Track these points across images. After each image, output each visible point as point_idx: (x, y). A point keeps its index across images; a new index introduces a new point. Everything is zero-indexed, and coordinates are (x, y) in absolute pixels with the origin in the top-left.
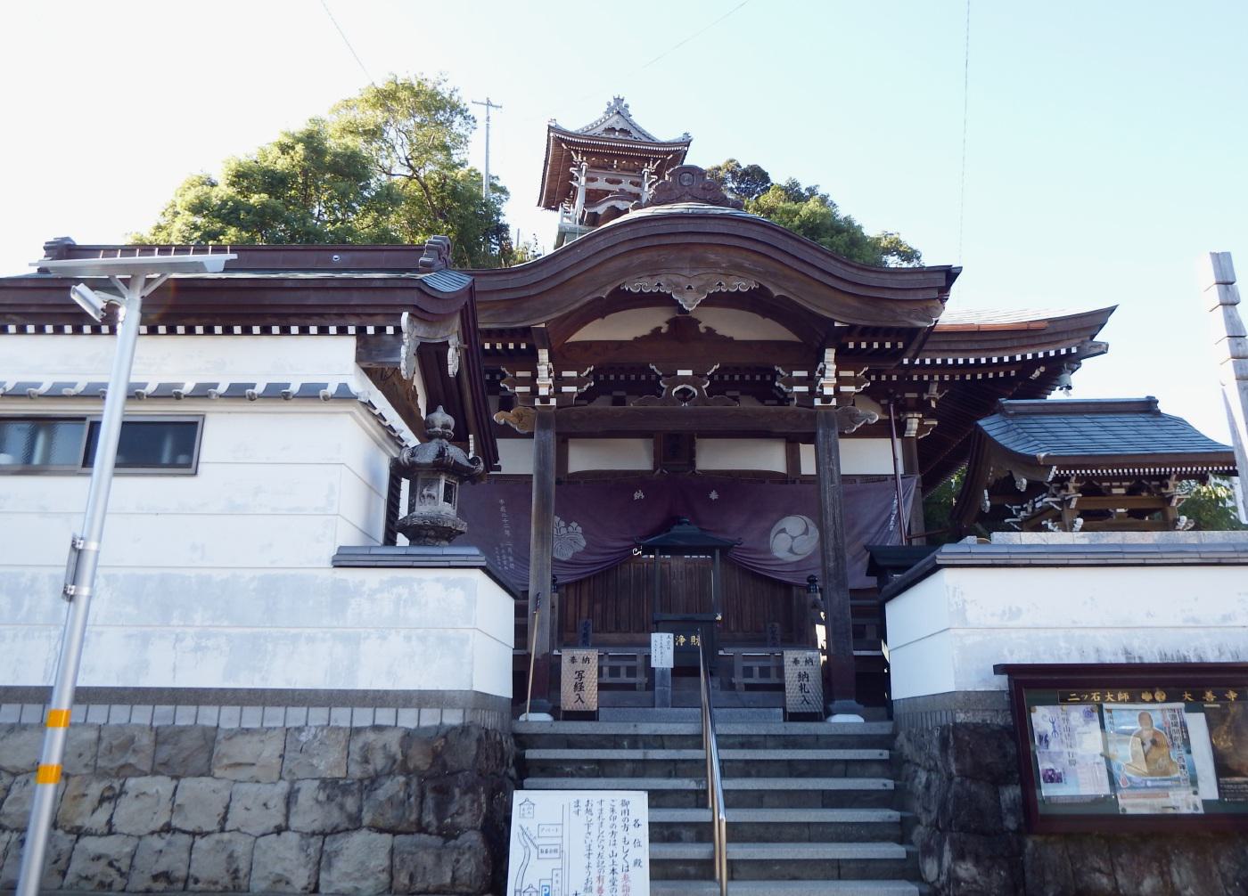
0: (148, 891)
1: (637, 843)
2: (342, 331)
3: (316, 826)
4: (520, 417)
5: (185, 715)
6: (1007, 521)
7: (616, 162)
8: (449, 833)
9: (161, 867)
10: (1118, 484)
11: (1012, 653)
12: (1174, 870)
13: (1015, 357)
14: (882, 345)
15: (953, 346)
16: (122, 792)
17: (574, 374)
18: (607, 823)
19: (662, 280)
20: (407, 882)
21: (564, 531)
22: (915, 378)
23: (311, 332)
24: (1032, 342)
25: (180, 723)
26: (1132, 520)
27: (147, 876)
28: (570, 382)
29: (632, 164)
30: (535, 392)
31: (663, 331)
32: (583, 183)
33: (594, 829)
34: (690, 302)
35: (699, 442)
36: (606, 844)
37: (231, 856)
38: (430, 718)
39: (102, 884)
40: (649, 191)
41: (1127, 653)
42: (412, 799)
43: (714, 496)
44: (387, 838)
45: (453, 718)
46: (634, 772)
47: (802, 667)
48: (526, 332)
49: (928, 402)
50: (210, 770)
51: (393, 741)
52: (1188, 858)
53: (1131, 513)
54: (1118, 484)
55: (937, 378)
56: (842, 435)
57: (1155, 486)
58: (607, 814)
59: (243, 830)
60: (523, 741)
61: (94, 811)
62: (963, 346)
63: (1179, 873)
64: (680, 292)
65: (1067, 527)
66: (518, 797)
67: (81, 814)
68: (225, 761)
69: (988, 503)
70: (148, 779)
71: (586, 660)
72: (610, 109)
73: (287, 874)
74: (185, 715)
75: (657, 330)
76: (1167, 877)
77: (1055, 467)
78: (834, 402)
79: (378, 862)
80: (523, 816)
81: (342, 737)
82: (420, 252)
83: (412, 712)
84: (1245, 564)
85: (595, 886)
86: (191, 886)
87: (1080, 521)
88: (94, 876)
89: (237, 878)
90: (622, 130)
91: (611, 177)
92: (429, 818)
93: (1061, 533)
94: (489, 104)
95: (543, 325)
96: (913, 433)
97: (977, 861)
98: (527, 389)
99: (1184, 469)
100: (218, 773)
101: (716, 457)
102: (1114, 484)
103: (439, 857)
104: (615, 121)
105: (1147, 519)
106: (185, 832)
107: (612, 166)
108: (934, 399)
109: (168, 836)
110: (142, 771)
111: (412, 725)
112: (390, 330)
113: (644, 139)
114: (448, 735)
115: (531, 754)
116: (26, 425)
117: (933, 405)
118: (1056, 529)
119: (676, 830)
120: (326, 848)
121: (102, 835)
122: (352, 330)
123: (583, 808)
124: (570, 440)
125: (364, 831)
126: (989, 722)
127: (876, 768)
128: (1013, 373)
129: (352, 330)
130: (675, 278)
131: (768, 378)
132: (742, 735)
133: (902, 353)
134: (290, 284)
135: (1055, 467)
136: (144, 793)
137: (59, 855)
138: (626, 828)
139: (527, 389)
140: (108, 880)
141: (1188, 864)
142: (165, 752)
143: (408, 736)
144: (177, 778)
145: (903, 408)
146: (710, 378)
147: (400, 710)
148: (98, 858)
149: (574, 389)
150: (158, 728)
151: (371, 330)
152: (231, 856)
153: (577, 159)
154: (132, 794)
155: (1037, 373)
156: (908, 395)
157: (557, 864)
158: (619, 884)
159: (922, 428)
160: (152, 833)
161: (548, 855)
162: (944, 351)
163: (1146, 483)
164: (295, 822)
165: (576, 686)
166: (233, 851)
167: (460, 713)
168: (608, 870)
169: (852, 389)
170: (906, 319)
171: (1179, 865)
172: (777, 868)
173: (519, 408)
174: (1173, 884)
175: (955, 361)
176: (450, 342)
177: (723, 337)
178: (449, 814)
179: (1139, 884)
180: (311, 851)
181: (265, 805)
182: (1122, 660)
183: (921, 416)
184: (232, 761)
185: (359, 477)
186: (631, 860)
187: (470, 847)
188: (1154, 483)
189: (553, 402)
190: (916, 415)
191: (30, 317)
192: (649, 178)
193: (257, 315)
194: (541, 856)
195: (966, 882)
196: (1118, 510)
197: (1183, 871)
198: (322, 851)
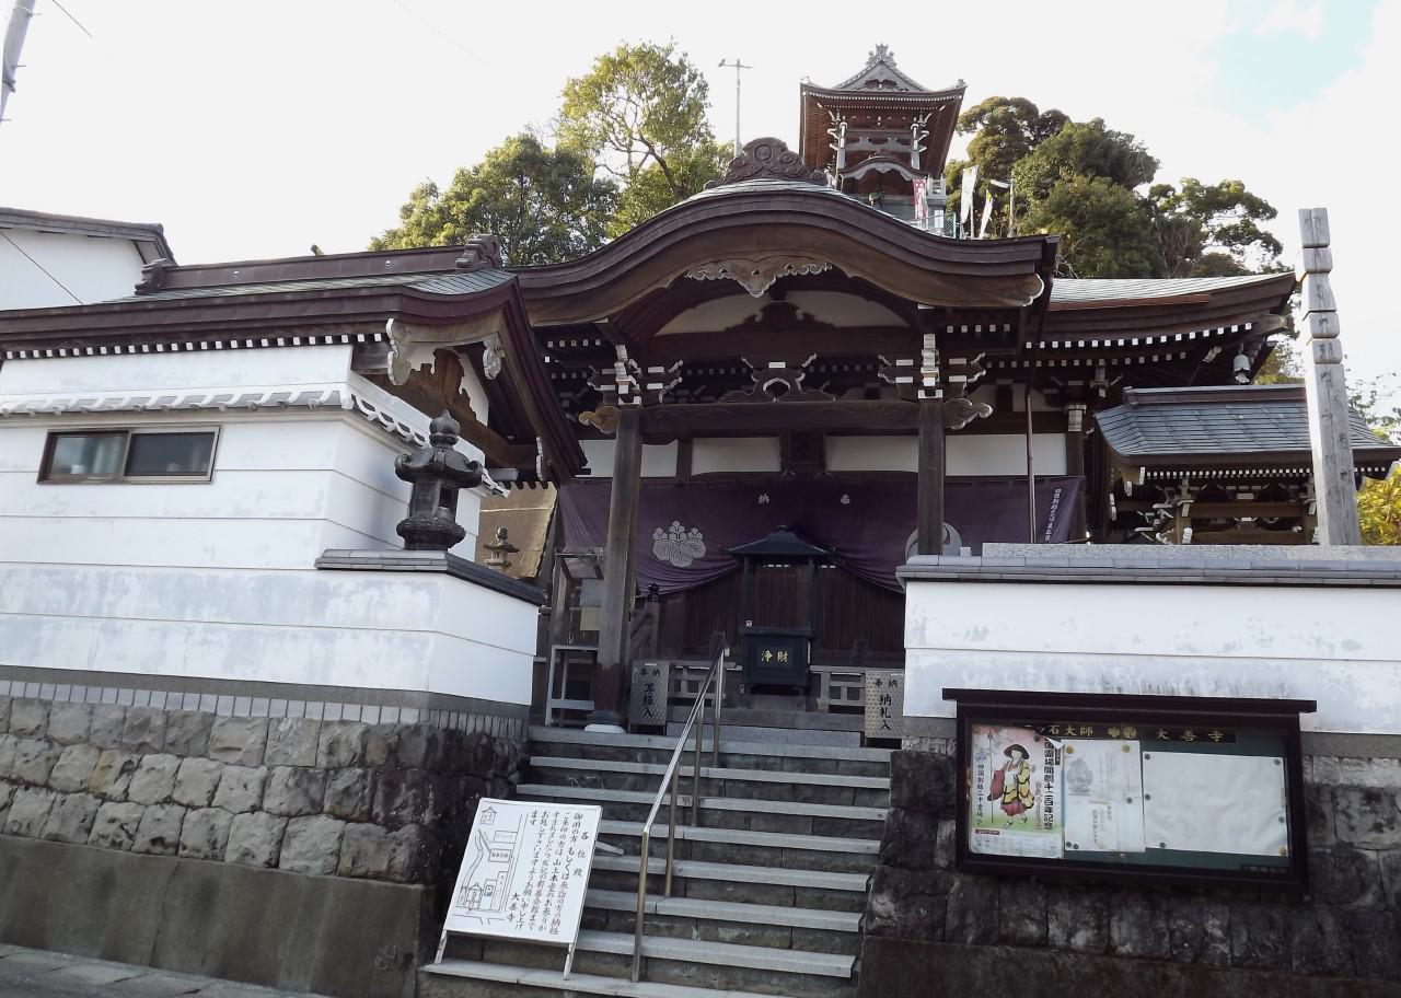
0: (148, 852)
1: (581, 854)
2: (337, 341)
3: (284, 808)
4: (603, 417)
5: (191, 702)
6: (1137, 530)
7: (879, 118)
8: (392, 824)
9: (156, 834)
10: (1247, 487)
11: (971, 677)
12: (1114, 923)
14: (985, 329)
15: (1099, 326)
16: (139, 766)
17: (660, 370)
18: (558, 833)
19: (727, 265)
20: (349, 865)
21: (683, 536)
23: (311, 343)
24: (1195, 318)
25: (187, 709)
26: (1261, 531)
27: (147, 839)
28: (958, 370)
30: (918, 384)
31: (757, 319)
32: (916, 147)
33: (545, 839)
34: (755, 288)
35: (828, 439)
36: (552, 852)
37: (212, 828)
38: (389, 716)
39: (114, 843)
40: (919, 149)
41: (1105, 682)
42: (367, 790)
43: (845, 500)
44: (340, 824)
45: (410, 717)
46: (635, 785)
48: (591, 330)
49: (1096, 390)
50: (206, 752)
51: (355, 734)
52: (1133, 912)
53: (1259, 523)
56: (948, 432)
57: (1231, 491)
58: (559, 825)
59: (226, 806)
60: (535, 747)
61: (116, 780)
62: (1110, 326)
63: (1119, 928)
64: (746, 278)
65: (1176, 539)
66: (485, 803)
67: (106, 783)
68: (219, 745)
69: (1114, 509)
70: (159, 757)
71: (656, 672)
72: (873, 59)
73: (253, 849)
74: (191, 702)
76: (1104, 932)
78: (939, 394)
79: (329, 845)
80: (483, 822)
81: (313, 730)
82: (460, 253)
84: (1398, 587)
85: (535, 890)
86: (181, 852)
88: (108, 836)
89: (214, 848)
90: (887, 83)
91: (876, 137)
92: (378, 809)
93: (1171, 545)
95: (606, 321)
97: (896, 898)
98: (910, 380)
99: (1234, 472)
101: (849, 458)
102: (1242, 488)
103: (379, 845)
104: (880, 74)
106: (180, 804)
109: (167, 807)
110: (153, 749)
111: (373, 722)
112: (378, 337)
113: (911, 90)
114: (404, 734)
115: (536, 761)
116: (80, 441)
117: (1102, 393)
118: (1164, 540)
119: (758, 853)
120: (288, 828)
121: (120, 802)
122: (345, 339)
123: (539, 818)
124: (695, 440)
125: (323, 817)
126: (936, 751)
128: (1183, 355)
129: (345, 339)
130: (740, 264)
131: (870, 367)
132: (758, 756)
134: (218, 302)
136: (153, 769)
137: (86, 816)
138: (574, 839)
139: (910, 380)
140: (118, 840)
141: (1131, 919)
142: (173, 734)
143: (368, 731)
144: (181, 757)
145: (1065, 398)
146: (806, 370)
147: (365, 707)
148: (113, 821)
149: (963, 378)
150: (169, 712)
151: (361, 338)
152: (212, 828)
153: (835, 118)
154: (145, 768)
156: (1072, 383)
157: (505, 867)
158: (557, 889)
160: (157, 803)
161: (499, 859)
162: (1127, 330)
163: (1284, 487)
164: (267, 804)
165: (645, 699)
166: (213, 826)
167: (415, 712)
168: (550, 876)
170: (999, 299)
171: (1121, 919)
172: (730, 889)
173: (604, 407)
174: (1110, 938)
175: (1101, 344)
177: (729, 330)
178: (395, 806)
179: (1070, 935)
180: (275, 830)
181: (245, 786)
182: (1099, 690)
183: (1085, 407)
184: (223, 746)
185: (371, 488)
186: (572, 869)
187: (407, 839)
188: (1292, 487)
189: (637, 400)
190: (1078, 407)
192: (919, 134)
193: (281, 328)
194: (492, 858)
195: (880, 916)
196: (1244, 519)
197: (1124, 925)
198: (284, 830)
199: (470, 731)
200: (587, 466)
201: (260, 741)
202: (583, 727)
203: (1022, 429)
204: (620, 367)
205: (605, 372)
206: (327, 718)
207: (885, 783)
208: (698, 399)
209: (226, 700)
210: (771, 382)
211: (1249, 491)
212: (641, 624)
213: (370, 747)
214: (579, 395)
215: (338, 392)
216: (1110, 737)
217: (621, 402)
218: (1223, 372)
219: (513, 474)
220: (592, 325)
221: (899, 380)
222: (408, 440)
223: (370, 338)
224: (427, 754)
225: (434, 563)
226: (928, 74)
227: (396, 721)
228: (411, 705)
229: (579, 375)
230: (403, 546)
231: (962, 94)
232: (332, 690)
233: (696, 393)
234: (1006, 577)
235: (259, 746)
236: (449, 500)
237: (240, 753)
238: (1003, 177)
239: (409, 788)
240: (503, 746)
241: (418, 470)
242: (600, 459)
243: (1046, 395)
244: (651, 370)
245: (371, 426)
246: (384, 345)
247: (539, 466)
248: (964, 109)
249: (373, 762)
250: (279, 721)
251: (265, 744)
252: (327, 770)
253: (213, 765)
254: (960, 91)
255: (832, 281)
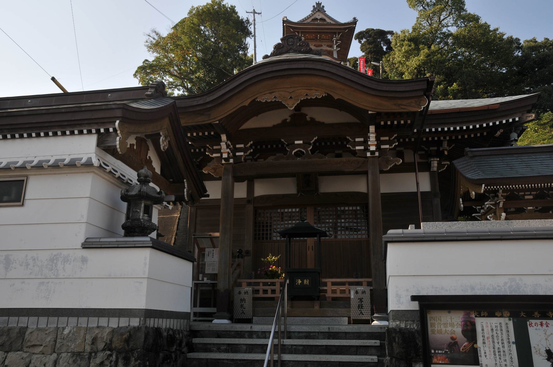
2: (89, 132)
6: (473, 215)
10: (529, 193)
13: (476, 126)
17: (242, 146)
19: (276, 94)
22: (424, 139)
28: (385, 143)
29: (327, 37)
30: (367, 149)
31: (288, 121)
32: (335, 48)
38: (124, 322)
45: (135, 322)
47: (360, 295)
48: (210, 127)
50: (22, 348)
51: (105, 335)
54: (529, 193)
55: (448, 138)
56: (382, 172)
60: (195, 333)
65: (497, 217)
68: (29, 344)
69: (462, 206)
75: (284, 121)
77: (483, 185)
78: (377, 154)
83: (116, 319)
87: (504, 215)
90: (322, 19)
94: (254, 12)
95: (218, 122)
96: (435, 169)
98: (362, 148)
100: (25, 349)
102: (526, 193)
104: (319, 16)
105: (551, 212)
107: (317, 38)
108: (446, 150)
111: (115, 326)
112: (111, 130)
113: (332, 22)
117: (446, 153)
122: (94, 131)
124: (255, 180)
127: (373, 351)
129: (94, 131)
131: (202, 150)
133: (411, 126)
135: (483, 185)
139: (362, 148)
143: (113, 331)
144: (7, 352)
145: (429, 155)
151: (102, 130)
155: (498, 133)
156: (431, 148)
159: (440, 166)
169: (387, 146)
175: (449, 129)
176: (161, 133)
177: (319, 122)
183: (438, 159)
189: (231, 161)
191: (33, 128)
192: (336, 43)
196: (529, 208)
199: (164, 327)
200: (207, 193)
201: (53, 340)
202: (211, 321)
203: (414, 171)
204: (223, 145)
205: (215, 147)
206: (90, 325)
207: (377, 343)
208: (256, 160)
209: (33, 319)
210: (296, 150)
211: (530, 195)
212: (235, 270)
213: (115, 339)
214: (198, 160)
215: (91, 158)
216: (497, 317)
217: (223, 162)
218: (505, 140)
219: (173, 198)
220: (210, 124)
221: (357, 148)
222: (125, 182)
223: (107, 130)
224: (145, 341)
225: (128, 243)
226: (339, 14)
227: (128, 325)
228: (135, 316)
229: (200, 150)
230: (123, 235)
231: (356, 24)
232: (324, 347)
233: (255, 158)
234: (437, 239)
235: (52, 343)
236: (148, 211)
237: (42, 347)
238: (378, 61)
239: (136, 360)
240: (179, 334)
241: (132, 196)
242: (214, 190)
243: (419, 154)
244: (238, 146)
245: (107, 175)
246: (114, 134)
247: (185, 193)
248: (357, 31)
249: (116, 347)
250: (64, 329)
251: (55, 341)
252: (90, 353)
253: (25, 355)
254: (355, 22)
255: (327, 102)
